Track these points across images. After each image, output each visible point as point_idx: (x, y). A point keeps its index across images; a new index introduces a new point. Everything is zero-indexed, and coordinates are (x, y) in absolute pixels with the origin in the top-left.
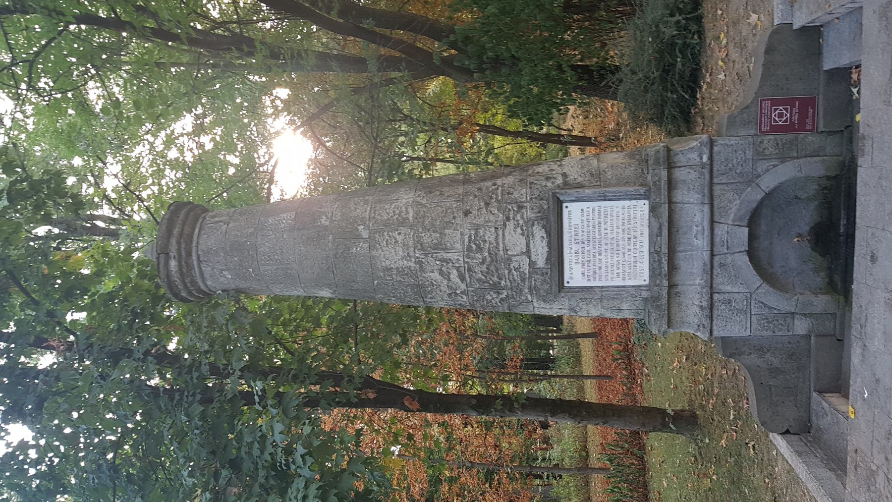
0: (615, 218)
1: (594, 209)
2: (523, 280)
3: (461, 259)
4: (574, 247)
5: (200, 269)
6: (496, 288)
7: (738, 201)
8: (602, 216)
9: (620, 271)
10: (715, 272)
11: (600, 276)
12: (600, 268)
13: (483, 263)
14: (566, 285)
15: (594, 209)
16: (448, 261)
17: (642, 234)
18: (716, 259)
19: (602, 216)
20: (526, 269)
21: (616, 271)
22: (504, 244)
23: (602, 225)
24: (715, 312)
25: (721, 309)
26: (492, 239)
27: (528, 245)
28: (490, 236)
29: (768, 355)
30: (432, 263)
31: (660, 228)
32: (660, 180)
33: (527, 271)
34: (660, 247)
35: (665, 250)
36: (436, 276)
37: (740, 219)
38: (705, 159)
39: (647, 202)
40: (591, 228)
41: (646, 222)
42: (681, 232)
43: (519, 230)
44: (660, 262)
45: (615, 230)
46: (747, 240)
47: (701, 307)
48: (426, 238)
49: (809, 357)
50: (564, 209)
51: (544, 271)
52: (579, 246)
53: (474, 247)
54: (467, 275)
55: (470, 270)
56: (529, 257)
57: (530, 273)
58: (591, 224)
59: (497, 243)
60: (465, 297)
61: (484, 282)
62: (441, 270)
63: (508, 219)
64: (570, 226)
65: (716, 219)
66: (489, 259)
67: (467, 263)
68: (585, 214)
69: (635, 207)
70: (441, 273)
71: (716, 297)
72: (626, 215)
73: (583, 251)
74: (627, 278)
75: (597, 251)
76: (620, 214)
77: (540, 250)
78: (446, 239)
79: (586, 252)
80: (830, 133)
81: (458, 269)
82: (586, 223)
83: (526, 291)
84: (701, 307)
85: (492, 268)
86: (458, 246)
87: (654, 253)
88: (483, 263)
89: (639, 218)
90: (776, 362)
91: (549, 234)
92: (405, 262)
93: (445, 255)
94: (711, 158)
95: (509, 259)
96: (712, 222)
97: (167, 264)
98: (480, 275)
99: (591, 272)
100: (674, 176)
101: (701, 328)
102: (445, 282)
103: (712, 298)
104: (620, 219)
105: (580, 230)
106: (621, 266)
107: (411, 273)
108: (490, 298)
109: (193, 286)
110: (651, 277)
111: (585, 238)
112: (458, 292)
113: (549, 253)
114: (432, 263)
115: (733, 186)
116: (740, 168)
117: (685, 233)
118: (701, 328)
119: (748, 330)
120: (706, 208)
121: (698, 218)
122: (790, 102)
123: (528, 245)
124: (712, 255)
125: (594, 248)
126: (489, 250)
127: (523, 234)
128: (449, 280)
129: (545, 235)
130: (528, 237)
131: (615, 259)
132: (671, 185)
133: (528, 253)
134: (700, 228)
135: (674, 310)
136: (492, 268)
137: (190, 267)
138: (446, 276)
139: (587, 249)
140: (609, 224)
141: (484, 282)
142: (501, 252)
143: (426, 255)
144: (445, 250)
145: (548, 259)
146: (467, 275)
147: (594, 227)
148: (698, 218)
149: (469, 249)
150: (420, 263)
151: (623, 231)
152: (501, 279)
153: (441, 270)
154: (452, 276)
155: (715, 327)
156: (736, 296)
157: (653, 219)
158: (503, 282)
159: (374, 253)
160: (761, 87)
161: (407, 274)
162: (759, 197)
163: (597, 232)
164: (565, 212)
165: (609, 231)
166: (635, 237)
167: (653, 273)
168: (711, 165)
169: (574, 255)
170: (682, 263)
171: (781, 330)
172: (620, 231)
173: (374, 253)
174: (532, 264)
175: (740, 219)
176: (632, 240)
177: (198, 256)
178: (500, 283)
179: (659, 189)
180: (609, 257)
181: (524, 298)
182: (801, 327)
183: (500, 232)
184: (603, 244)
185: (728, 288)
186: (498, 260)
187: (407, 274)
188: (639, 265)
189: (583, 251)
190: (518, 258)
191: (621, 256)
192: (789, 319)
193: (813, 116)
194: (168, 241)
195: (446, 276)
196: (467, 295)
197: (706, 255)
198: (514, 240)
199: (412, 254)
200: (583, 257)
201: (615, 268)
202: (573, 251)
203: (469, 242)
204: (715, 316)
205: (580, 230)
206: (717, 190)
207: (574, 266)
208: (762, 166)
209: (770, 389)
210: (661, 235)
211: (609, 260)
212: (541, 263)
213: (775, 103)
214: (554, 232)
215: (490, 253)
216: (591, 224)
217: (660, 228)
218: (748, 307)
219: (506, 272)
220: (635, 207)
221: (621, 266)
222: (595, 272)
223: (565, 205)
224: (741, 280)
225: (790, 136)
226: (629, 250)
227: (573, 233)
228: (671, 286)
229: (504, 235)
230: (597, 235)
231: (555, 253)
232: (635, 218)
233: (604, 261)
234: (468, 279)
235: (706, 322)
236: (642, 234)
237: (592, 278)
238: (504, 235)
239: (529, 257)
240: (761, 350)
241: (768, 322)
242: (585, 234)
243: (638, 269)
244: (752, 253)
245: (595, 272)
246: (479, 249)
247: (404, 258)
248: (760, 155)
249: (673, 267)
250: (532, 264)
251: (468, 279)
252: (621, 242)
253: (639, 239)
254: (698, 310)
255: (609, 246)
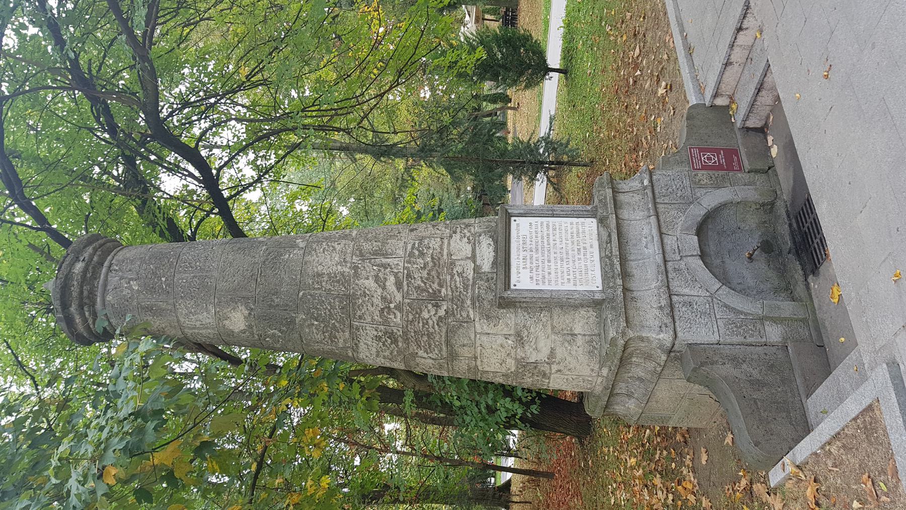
0: (563, 231)
1: (542, 223)
2: (466, 287)
3: (402, 264)
4: (522, 254)
5: (106, 280)
6: (435, 299)
7: (683, 218)
8: (551, 229)
9: (571, 277)
10: (670, 275)
11: (550, 281)
12: (550, 273)
13: (424, 268)
14: (512, 287)
15: (542, 223)
16: (385, 266)
17: (591, 246)
18: (670, 264)
19: (551, 229)
20: (470, 274)
21: (566, 277)
22: (449, 249)
23: (551, 236)
24: (676, 313)
25: (681, 311)
26: (436, 246)
27: (474, 251)
28: (435, 244)
29: (744, 366)
30: (369, 269)
31: (610, 235)
32: (605, 197)
33: (470, 277)
34: (611, 253)
35: (616, 252)
36: (371, 283)
37: (687, 229)
38: (646, 182)
39: (594, 220)
40: (539, 238)
41: (595, 236)
42: (630, 243)
43: (466, 240)
44: (612, 265)
45: (564, 241)
46: (697, 245)
47: (661, 308)
48: (366, 246)
49: (791, 369)
50: (513, 223)
51: (490, 276)
52: (528, 254)
53: (417, 253)
54: (405, 283)
55: (409, 276)
56: (474, 262)
57: (474, 278)
58: (539, 235)
59: (442, 249)
60: (398, 314)
61: (423, 290)
62: (377, 276)
63: (455, 232)
64: (518, 237)
65: (664, 230)
66: (431, 264)
67: (407, 268)
68: (534, 227)
69: (583, 223)
70: (377, 279)
71: (675, 298)
72: (575, 230)
73: (531, 258)
74: (578, 283)
75: (546, 257)
76: (569, 228)
77: (486, 254)
78: (388, 247)
79: (534, 259)
80: (757, 171)
81: (396, 275)
82: (534, 235)
83: (469, 302)
84: (661, 308)
85: (434, 273)
86: (401, 252)
87: (606, 259)
88: (424, 268)
89: (587, 232)
90: (756, 374)
91: (496, 242)
92: (339, 267)
93: (384, 261)
94: (651, 181)
95: (453, 263)
96: (661, 234)
97: (72, 265)
98: (420, 282)
99: (540, 276)
100: (618, 199)
101: (664, 329)
102: (380, 291)
103: (671, 300)
104: (569, 232)
105: (528, 240)
106: (571, 273)
107: (344, 280)
108: (427, 316)
109: (88, 297)
110: (603, 280)
111: (534, 247)
112: (392, 306)
113: (496, 258)
114: (369, 269)
115: (676, 206)
116: (679, 192)
117: (635, 245)
118: (664, 329)
119: (716, 334)
120: (653, 219)
121: (646, 231)
122: (717, 151)
123: (474, 251)
124: (665, 261)
125: (543, 256)
126: (432, 255)
127: (469, 243)
128: (384, 288)
129: (492, 243)
130: (474, 243)
131: (565, 266)
132: (617, 205)
133: (473, 258)
134: (649, 238)
135: (631, 313)
136: (434, 273)
137: (95, 276)
138: (381, 282)
139: (535, 256)
140: (558, 236)
141: (423, 290)
142: (445, 257)
143: (363, 260)
144: (386, 255)
145: (495, 263)
146: (405, 283)
147: (542, 238)
148: (646, 231)
149: (411, 254)
150: (356, 268)
151: (573, 243)
152: (442, 286)
153: (377, 276)
154: (387, 284)
155: (678, 329)
156: (696, 299)
157: (601, 229)
158: (443, 290)
159: (307, 258)
160: (687, 139)
161: (338, 282)
162: (703, 212)
163: (546, 242)
164: (513, 225)
165: (558, 242)
166: (585, 248)
167: (605, 277)
168: (652, 186)
169: (521, 260)
170: (634, 271)
171: (752, 336)
172: (569, 242)
173: (307, 258)
174: (477, 269)
175: (687, 229)
176: (582, 250)
177: (111, 265)
178: (440, 292)
179: (605, 205)
180: (559, 264)
181: (464, 314)
182: (774, 333)
183: (446, 241)
184: (552, 253)
185: (687, 291)
186: (440, 265)
187: (338, 282)
188: (590, 272)
189: (531, 258)
190: (462, 263)
191: (571, 263)
192: (759, 326)
193: (739, 161)
194: (84, 247)
195: (381, 282)
196: (401, 311)
197: (659, 259)
198: (460, 247)
199: (348, 259)
200: (531, 263)
201: (565, 274)
202: (521, 257)
203: (413, 248)
204: (677, 318)
205: (528, 240)
206: (661, 208)
207: (521, 270)
208: (699, 193)
209: (755, 402)
210: (611, 242)
211: (559, 267)
212: (486, 267)
213: (701, 150)
214: (502, 244)
215: (432, 258)
216: (539, 235)
217: (610, 235)
218: (713, 315)
219: (448, 277)
220: (583, 223)
221: (571, 273)
222: (544, 277)
223: (513, 219)
224: (697, 284)
225: (721, 173)
226: (579, 259)
227: (521, 242)
228: (626, 290)
229: (449, 243)
230: (545, 244)
231: (501, 254)
232: (584, 232)
233: (553, 267)
234: (405, 288)
235: (668, 321)
236: (591, 246)
237: (541, 283)
238: (449, 243)
239: (474, 262)
240: (735, 361)
241: (736, 327)
242: (534, 243)
243: (590, 276)
244: (703, 256)
245: (544, 277)
246: (422, 254)
247: (339, 263)
248: (697, 184)
249: (625, 275)
250: (477, 269)
251: (405, 288)
252: (570, 252)
253: (589, 250)
254: (657, 312)
255: (559, 255)
